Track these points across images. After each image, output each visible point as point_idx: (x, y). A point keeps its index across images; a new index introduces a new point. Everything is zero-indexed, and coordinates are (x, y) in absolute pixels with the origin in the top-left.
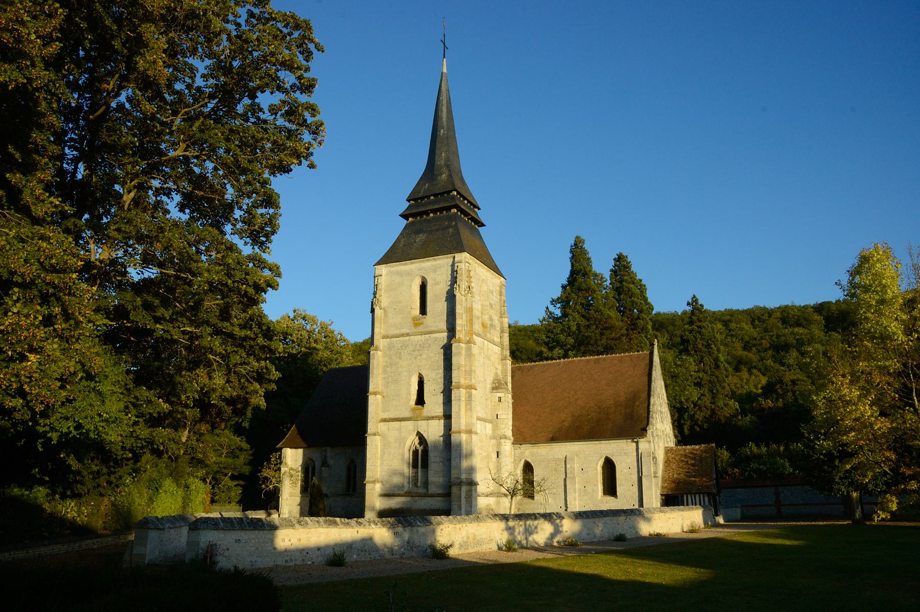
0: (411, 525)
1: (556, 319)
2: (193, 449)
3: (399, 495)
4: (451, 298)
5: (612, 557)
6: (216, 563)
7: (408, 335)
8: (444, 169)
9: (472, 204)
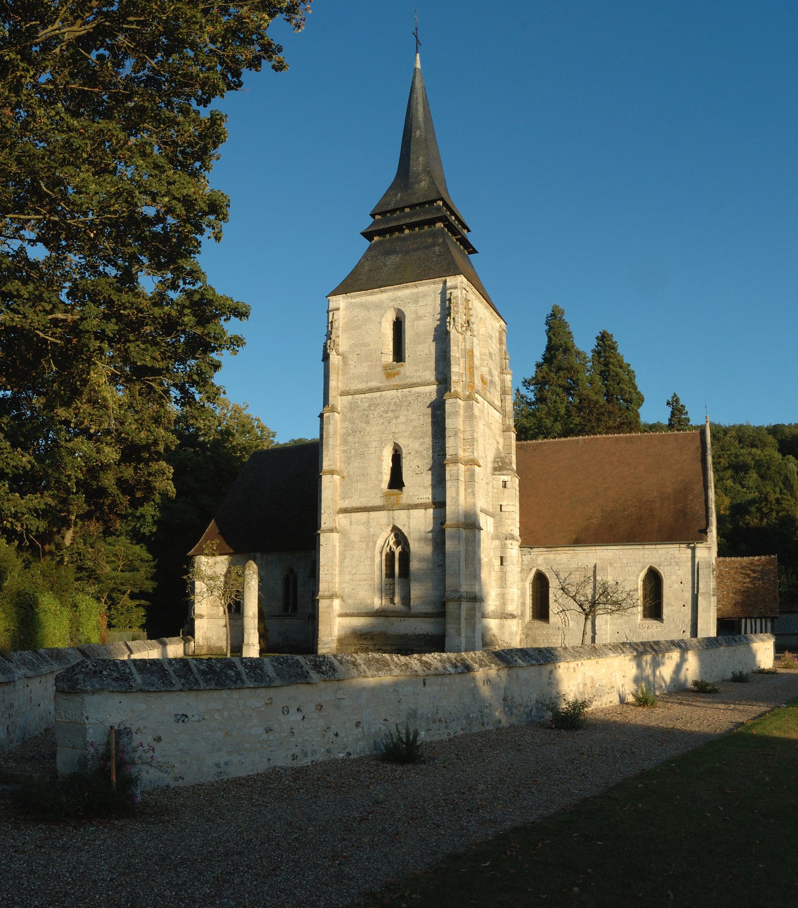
2: (80, 554)
4: (442, 337)
7: (378, 389)
8: (423, 176)
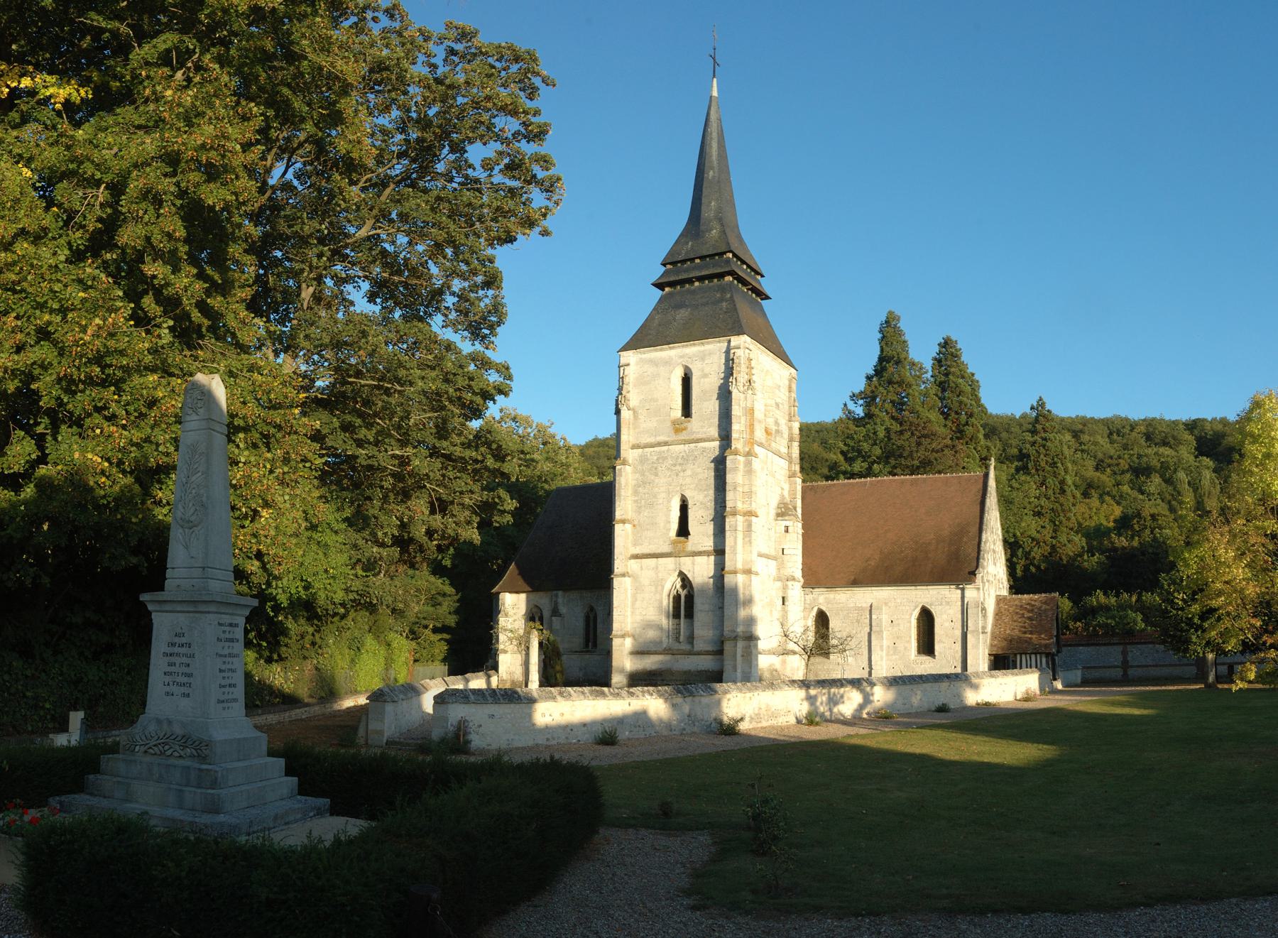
0: (692, 694)
1: (858, 422)
3: (655, 653)
4: (725, 396)
5: (939, 733)
6: (469, 742)
7: (666, 444)
8: (715, 224)
9: (753, 269)
